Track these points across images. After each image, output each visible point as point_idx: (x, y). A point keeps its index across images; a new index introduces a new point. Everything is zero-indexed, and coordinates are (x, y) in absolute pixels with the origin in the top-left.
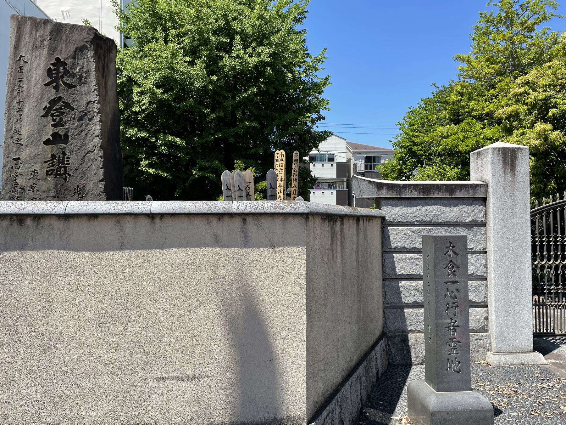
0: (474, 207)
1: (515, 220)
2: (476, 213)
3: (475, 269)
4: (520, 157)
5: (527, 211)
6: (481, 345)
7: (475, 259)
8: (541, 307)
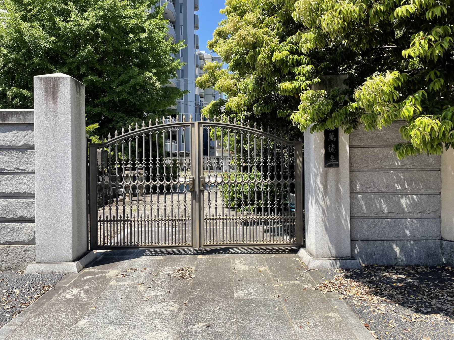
0: (27, 132)
1: (56, 143)
2: (28, 137)
3: (27, 188)
4: (61, 86)
5: (68, 135)
6: (28, 256)
7: (28, 179)
8: (126, 222)
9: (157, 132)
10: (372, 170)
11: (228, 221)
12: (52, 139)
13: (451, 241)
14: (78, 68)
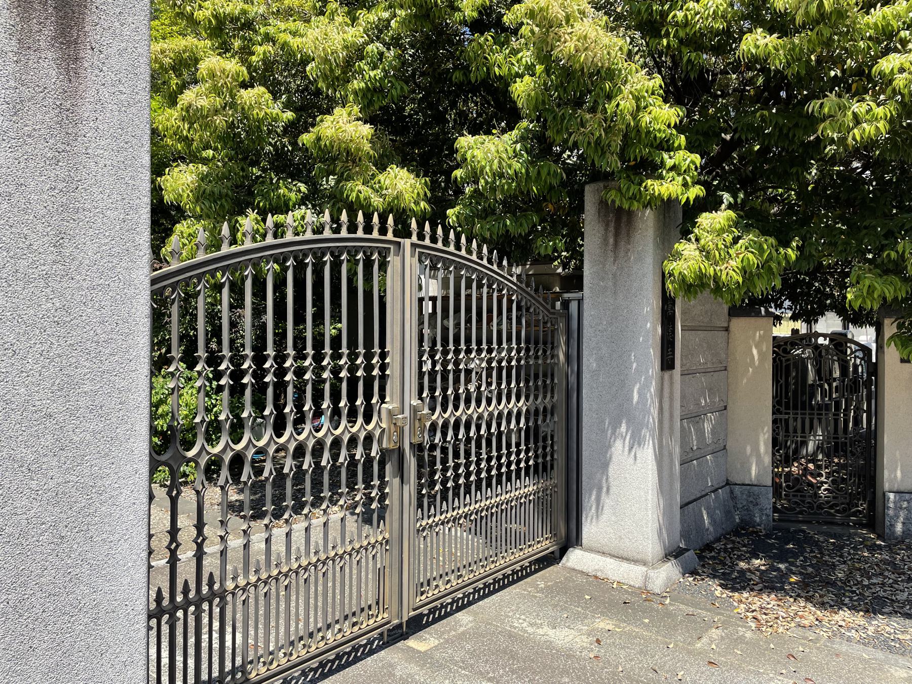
5: (137, 247)
9: (327, 258)
10: (703, 371)
11: (263, 590)
12: (51, 257)
13: (743, 485)
14: (745, 115)
